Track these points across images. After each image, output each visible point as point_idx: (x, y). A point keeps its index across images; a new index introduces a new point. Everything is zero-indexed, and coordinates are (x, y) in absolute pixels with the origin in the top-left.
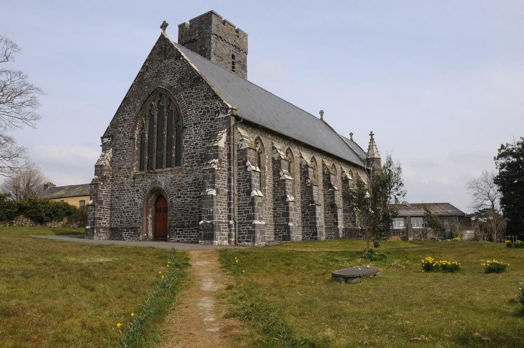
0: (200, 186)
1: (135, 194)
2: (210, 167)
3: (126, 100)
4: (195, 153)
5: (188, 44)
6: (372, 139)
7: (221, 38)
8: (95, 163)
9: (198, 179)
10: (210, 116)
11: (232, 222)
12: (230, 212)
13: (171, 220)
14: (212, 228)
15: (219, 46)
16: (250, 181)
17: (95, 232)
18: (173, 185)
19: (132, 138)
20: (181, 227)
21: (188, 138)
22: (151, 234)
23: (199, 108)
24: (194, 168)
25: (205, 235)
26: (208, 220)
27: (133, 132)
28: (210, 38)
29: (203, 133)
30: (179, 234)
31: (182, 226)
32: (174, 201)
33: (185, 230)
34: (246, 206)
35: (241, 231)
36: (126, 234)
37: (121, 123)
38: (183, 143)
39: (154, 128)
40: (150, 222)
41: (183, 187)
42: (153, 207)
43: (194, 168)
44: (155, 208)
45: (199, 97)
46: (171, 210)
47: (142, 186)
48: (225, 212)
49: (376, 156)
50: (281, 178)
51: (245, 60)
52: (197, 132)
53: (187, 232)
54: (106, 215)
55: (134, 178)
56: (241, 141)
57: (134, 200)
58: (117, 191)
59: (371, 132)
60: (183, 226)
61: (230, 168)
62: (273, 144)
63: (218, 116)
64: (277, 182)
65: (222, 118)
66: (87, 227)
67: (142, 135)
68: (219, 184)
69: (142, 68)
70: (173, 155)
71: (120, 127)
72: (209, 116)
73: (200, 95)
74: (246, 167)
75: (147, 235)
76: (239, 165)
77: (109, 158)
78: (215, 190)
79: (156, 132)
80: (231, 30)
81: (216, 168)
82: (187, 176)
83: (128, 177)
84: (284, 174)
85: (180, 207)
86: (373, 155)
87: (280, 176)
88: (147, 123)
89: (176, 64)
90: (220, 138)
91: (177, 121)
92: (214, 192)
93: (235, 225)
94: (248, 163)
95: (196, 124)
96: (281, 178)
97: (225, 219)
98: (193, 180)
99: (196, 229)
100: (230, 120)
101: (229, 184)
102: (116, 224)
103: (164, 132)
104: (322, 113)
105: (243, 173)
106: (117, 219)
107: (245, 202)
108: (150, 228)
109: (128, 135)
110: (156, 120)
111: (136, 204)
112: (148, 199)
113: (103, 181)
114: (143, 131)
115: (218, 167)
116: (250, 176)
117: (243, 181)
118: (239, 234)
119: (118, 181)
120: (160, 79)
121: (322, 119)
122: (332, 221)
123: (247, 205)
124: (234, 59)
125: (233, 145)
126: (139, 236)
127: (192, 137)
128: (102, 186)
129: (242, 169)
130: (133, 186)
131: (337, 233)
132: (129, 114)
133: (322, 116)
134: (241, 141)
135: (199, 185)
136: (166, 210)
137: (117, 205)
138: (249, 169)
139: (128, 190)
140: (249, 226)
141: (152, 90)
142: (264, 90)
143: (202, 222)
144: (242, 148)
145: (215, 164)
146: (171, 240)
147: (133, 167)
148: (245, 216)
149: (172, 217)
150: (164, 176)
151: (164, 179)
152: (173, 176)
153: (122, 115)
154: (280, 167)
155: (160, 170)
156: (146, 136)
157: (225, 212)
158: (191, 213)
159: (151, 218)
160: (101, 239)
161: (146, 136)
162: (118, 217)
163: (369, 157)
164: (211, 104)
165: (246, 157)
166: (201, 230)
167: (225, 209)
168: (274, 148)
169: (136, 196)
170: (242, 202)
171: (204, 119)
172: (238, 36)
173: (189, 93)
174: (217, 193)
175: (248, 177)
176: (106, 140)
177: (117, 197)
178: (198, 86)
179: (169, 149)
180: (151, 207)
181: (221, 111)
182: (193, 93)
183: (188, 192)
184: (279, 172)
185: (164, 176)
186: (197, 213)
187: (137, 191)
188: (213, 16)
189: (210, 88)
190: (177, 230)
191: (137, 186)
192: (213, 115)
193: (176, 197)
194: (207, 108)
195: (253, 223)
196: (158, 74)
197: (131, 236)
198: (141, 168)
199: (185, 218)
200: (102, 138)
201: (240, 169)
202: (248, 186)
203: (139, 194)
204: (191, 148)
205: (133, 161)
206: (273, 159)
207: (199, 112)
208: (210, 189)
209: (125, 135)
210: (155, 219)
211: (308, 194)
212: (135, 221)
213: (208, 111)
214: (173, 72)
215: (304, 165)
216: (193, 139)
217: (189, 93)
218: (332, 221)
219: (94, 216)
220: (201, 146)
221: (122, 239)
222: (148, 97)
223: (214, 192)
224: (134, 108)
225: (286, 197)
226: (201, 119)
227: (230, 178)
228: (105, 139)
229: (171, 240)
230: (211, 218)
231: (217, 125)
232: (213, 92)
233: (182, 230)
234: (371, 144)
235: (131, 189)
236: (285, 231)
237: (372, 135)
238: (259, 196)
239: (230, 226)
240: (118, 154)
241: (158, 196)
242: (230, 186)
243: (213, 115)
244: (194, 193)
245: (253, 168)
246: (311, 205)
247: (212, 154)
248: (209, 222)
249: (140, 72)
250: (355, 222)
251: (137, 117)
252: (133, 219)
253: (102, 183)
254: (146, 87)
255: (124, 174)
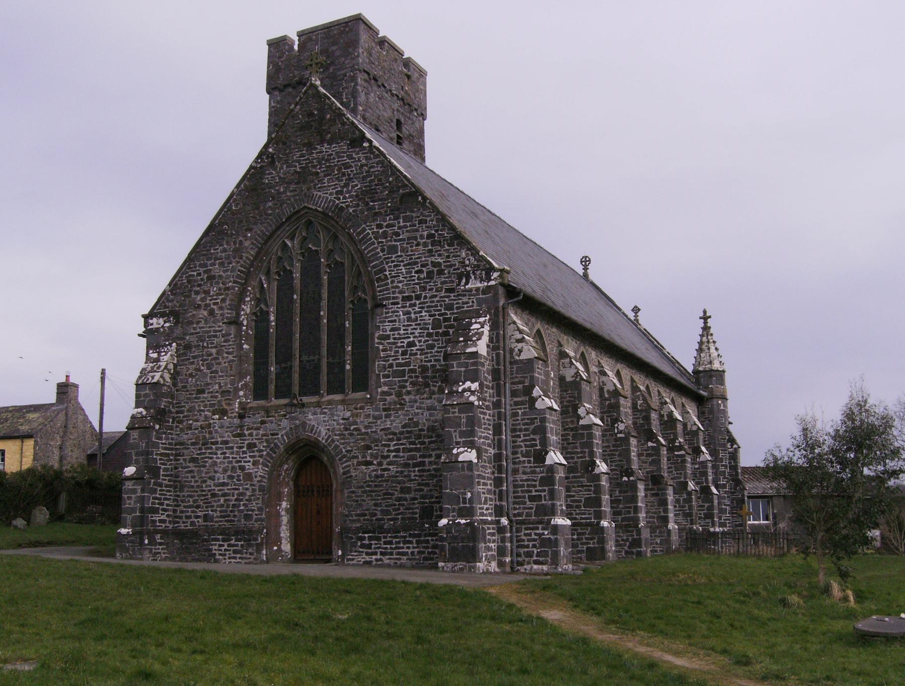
0: (437, 438)
1: (244, 452)
2: (462, 400)
3: (215, 232)
4: (408, 364)
5: (294, 88)
6: (706, 328)
7: (375, 79)
8: (134, 381)
9: (417, 424)
10: (445, 282)
11: (504, 521)
12: (501, 499)
13: (347, 516)
14: (473, 534)
15: (372, 97)
16: (541, 430)
17: (146, 542)
18: (351, 435)
19: (235, 322)
20: (374, 532)
21: (388, 328)
22: (286, 547)
23: (416, 263)
24: (407, 398)
25: (453, 550)
26: (461, 516)
27: (237, 308)
28: (353, 79)
29: (429, 320)
30: (369, 546)
31: (377, 530)
32: (353, 470)
33: (385, 537)
34: (535, 486)
35: (523, 541)
36: (221, 546)
37: (199, 285)
38: (376, 341)
39: (292, 300)
40: (285, 519)
41: (376, 440)
42: (291, 483)
43: (407, 398)
44: (296, 485)
45: (415, 238)
46: (346, 491)
47: (263, 435)
48: (491, 500)
49: (716, 366)
50: (582, 422)
51: (421, 132)
52: (413, 316)
53: (390, 543)
54: (166, 502)
55: (241, 417)
56: (518, 341)
57: (242, 468)
58: (193, 444)
59: (705, 312)
60: (381, 529)
61: (499, 401)
62: (560, 345)
63: (467, 283)
64: (572, 429)
65: (477, 289)
66: (124, 531)
67: (260, 318)
68: (480, 438)
69: (257, 158)
70: (348, 367)
71: (197, 293)
72: (445, 282)
73: (418, 234)
74: (533, 400)
75: (280, 550)
76: (514, 394)
77: (171, 366)
78: (474, 451)
79: (298, 311)
80: (396, 60)
81: (476, 403)
82: (387, 416)
83: (223, 413)
84: (588, 413)
85: (369, 486)
86: (711, 363)
87: (579, 418)
88: (273, 290)
89: (350, 157)
90: (480, 335)
91: (355, 289)
92: (471, 456)
93: (511, 527)
94: (537, 391)
95: (409, 298)
96: (582, 422)
97: (490, 514)
98: (404, 426)
99: (414, 536)
100: (496, 295)
101: (496, 438)
102: (193, 524)
103: (322, 313)
104: (585, 262)
105: (524, 414)
106: (192, 512)
107: (530, 477)
108: (285, 533)
109: (222, 315)
110: (297, 282)
111: (249, 477)
112: (281, 466)
113: (159, 421)
114: (263, 306)
115: (479, 399)
116: (543, 420)
117: (526, 430)
118: (518, 547)
119: (197, 421)
120: (309, 189)
121: (586, 276)
122: (655, 513)
123: (537, 483)
124: (401, 132)
125: (504, 350)
126: (259, 551)
127: (401, 330)
128: (157, 431)
129: (522, 403)
130: (239, 435)
131: (667, 541)
132: (222, 264)
133: (586, 268)
134: (518, 341)
135: (419, 437)
136: (326, 491)
137: (193, 477)
138: (539, 405)
139: (226, 442)
140: (543, 529)
141: (288, 211)
142: (489, 211)
143: (444, 522)
144: (521, 358)
145: (473, 393)
146: (349, 560)
147: (237, 390)
148: (532, 508)
149: (343, 508)
150: (325, 413)
151: (324, 421)
152: (348, 414)
153: (201, 266)
154: (579, 398)
155: (314, 399)
156: (272, 318)
157: (491, 500)
158: (399, 499)
159: (287, 510)
160: (158, 557)
161: (272, 318)
162: (198, 507)
163: (701, 369)
164: (448, 257)
165: (532, 377)
166: (442, 539)
167: (489, 492)
168: (563, 355)
169: (248, 459)
170: (525, 477)
171: (431, 290)
172: (409, 77)
173: (387, 226)
174: (479, 457)
175: (537, 423)
176: (156, 323)
177: (193, 460)
178: (413, 212)
179: (336, 350)
180: (287, 484)
181: (474, 274)
182: (399, 228)
183: (392, 451)
184: (576, 408)
185: (325, 413)
186: (414, 499)
187: (251, 446)
188: (362, 27)
189: (443, 219)
190: (363, 539)
191: (251, 435)
192: (452, 282)
193: (359, 464)
194: (434, 264)
195: (552, 523)
196: (304, 177)
197: (235, 552)
198: (260, 391)
199: (382, 511)
200: (146, 317)
201: (516, 404)
202: (538, 442)
203: (256, 454)
204: (397, 352)
205: (242, 376)
206: (562, 379)
207: (417, 272)
208: (462, 449)
209: (212, 313)
210: (296, 513)
211: (620, 455)
212: (248, 517)
213: (441, 272)
214: (344, 174)
215: (608, 391)
216: (402, 332)
217: (387, 226)
218: (655, 513)
219: (143, 504)
220: (422, 350)
221: (210, 557)
222: (278, 228)
223: (471, 456)
224: (236, 251)
225: (593, 464)
226: (424, 289)
227: (500, 424)
228: (154, 321)
229: (349, 560)
230: (468, 512)
231: (463, 303)
232: (453, 228)
233: (378, 539)
234: (705, 339)
235: (235, 442)
236: (591, 539)
237: (705, 318)
238: (561, 464)
239: (501, 530)
240: (194, 357)
241: (308, 461)
242: (500, 441)
243: (452, 282)
244: (406, 455)
245: (548, 402)
246: (625, 479)
247: (463, 369)
248: (463, 521)
249: (251, 167)
250: (690, 515)
251: (247, 275)
252: (240, 511)
253: (157, 427)
254: (270, 204)
255: (212, 405)
